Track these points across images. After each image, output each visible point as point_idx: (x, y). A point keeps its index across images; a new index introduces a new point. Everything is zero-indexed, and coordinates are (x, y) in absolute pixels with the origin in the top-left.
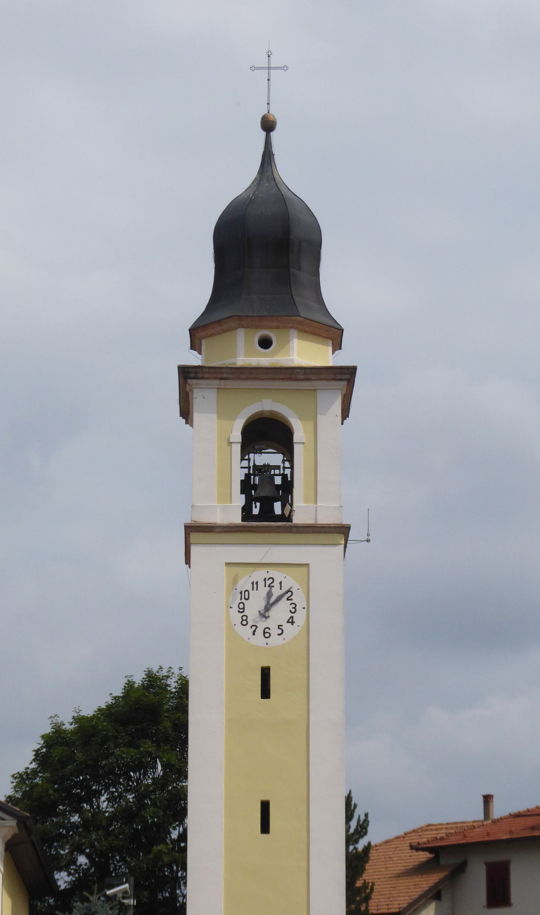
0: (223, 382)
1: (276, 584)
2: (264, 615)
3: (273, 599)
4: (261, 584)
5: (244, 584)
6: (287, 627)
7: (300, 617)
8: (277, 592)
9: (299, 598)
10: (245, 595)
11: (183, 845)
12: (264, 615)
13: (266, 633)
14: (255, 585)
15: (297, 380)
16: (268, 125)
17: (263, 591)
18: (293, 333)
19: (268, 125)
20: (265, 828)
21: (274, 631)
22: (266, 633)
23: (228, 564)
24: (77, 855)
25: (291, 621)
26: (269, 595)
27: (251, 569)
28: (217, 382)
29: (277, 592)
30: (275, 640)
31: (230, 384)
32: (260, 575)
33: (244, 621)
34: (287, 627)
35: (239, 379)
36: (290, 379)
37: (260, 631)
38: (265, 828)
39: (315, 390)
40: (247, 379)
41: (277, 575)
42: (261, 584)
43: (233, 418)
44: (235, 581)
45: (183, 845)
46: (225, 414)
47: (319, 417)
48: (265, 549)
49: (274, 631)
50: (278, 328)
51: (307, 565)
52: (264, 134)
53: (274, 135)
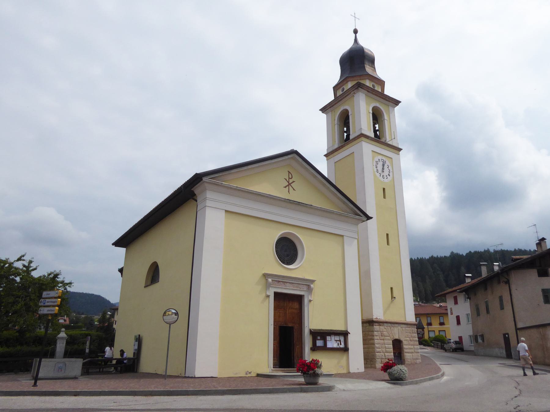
6: (388, 176)
16: (356, 32)
19: (356, 32)
28: (366, 92)
35: (372, 93)
37: (382, 176)
48: (381, 149)
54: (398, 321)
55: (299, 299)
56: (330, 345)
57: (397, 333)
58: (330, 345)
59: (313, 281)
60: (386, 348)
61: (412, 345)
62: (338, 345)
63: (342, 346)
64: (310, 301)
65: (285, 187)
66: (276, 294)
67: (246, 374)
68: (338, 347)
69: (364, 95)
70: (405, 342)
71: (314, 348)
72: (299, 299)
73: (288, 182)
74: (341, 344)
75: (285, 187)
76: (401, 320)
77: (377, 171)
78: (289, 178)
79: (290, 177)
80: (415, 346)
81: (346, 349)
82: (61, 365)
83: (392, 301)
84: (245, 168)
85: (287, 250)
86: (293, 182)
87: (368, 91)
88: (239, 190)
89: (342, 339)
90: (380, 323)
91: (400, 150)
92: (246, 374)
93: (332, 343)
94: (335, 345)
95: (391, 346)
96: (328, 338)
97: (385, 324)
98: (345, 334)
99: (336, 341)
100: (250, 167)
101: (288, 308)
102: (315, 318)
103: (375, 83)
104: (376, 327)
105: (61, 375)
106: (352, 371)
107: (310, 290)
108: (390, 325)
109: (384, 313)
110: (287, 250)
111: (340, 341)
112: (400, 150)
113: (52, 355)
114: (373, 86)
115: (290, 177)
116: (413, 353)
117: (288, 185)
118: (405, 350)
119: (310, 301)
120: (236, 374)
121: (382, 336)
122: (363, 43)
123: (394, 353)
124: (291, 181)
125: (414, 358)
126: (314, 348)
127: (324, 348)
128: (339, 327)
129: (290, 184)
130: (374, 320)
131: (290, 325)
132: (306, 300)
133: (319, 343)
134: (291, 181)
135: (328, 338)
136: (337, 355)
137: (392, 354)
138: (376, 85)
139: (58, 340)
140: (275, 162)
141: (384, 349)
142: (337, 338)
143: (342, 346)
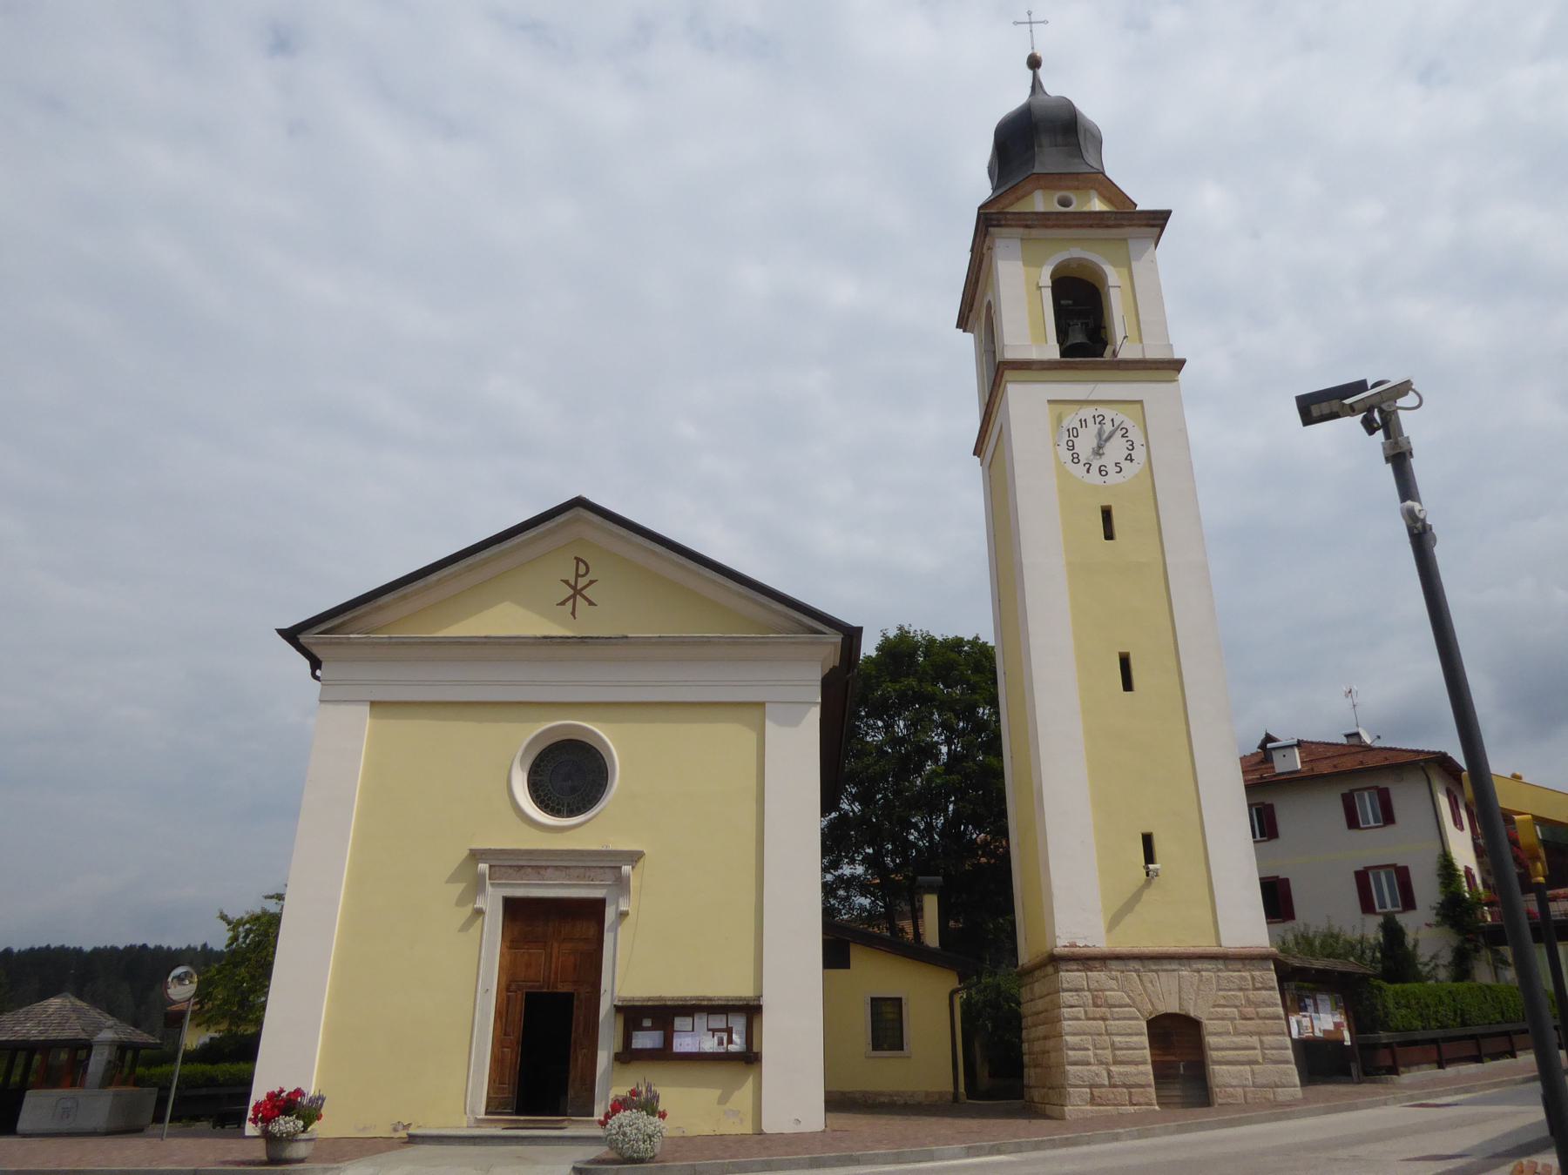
0: (1027, 231)
1: (1107, 421)
2: (1098, 451)
3: (1105, 436)
4: (1090, 421)
5: (1071, 421)
6: (1125, 465)
7: (1139, 454)
8: (1108, 428)
9: (1135, 435)
10: (1073, 433)
11: (829, 877)
12: (1098, 451)
13: (1102, 471)
14: (1084, 423)
15: (1108, 226)
16: (1034, 63)
17: (1093, 428)
18: (1093, 193)
19: (1034, 63)
20: (1128, 685)
21: (1112, 469)
22: (1102, 471)
23: (1049, 402)
24: (859, 755)
25: (1130, 458)
26: (1100, 434)
27: (1076, 407)
28: (1021, 230)
29: (1108, 428)
30: (1113, 478)
31: (1034, 232)
32: (1087, 412)
33: (1076, 459)
34: (1125, 465)
35: (1046, 227)
36: (1099, 226)
37: (1094, 469)
38: (1128, 685)
39: (762, 704)
40: (1053, 226)
41: (1109, 412)
42: (1090, 421)
43: (1040, 265)
44: (1059, 419)
45: (829, 877)
46: (1031, 262)
47: (1134, 264)
48: (1090, 386)
49: (1112, 469)
50: (1077, 188)
51: (1141, 402)
52: (1030, 73)
53: (1041, 72)
54: (1181, 950)
55: (593, 911)
57: (1169, 993)
58: (683, 1044)
59: (635, 857)
60: (1114, 1047)
61: (1251, 1034)
62: (721, 1043)
63: (738, 1044)
64: (624, 915)
65: (563, 603)
66: (513, 908)
67: (395, 1130)
68: (721, 1050)
69: (1016, 245)
70: (1209, 1025)
71: (627, 1056)
72: (593, 911)
73: (574, 588)
74: (730, 1041)
75: (563, 603)
76: (1205, 944)
77: (1076, 459)
78: (577, 575)
80: (1268, 1039)
81: (750, 1058)
82: (69, 1104)
83: (1148, 883)
84: (420, 583)
85: (568, 776)
86: (592, 582)
87: (1027, 226)
88: (397, 644)
89: (738, 1023)
90: (1087, 960)
91: (1178, 365)
92: (395, 1130)
93: (693, 1038)
94: (709, 1044)
95: (1145, 1040)
96: (680, 1023)
97: (1113, 964)
98: (751, 1011)
99: (714, 1031)
100: (433, 577)
101: (552, 940)
102: (633, 968)
103: (1068, 188)
104: (1070, 977)
105: (65, 1126)
106: (769, 1127)
107: (622, 884)
108: (1136, 965)
109: (1114, 922)
110: (568, 776)
112: (1178, 365)
114: (1065, 202)
115: (582, 569)
116: (1256, 1062)
117: (573, 597)
118: (1215, 1055)
119: (624, 915)
120: (364, 1129)
121: (1096, 1005)
122: (1054, 87)
123: (1154, 1063)
124: (582, 582)
125: (1259, 1081)
126: (627, 1056)
127: (664, 1054)
128: (736, 988)
129: (577, 592)
130: (1057, 951)
131: (563, 988)
132: (610, 914)
136: (721, 1073)
137: (1149, 1068)
138: (1071, 195)
141: (1107, 1054)
142: (719, 1022)
143: (738, 1044)
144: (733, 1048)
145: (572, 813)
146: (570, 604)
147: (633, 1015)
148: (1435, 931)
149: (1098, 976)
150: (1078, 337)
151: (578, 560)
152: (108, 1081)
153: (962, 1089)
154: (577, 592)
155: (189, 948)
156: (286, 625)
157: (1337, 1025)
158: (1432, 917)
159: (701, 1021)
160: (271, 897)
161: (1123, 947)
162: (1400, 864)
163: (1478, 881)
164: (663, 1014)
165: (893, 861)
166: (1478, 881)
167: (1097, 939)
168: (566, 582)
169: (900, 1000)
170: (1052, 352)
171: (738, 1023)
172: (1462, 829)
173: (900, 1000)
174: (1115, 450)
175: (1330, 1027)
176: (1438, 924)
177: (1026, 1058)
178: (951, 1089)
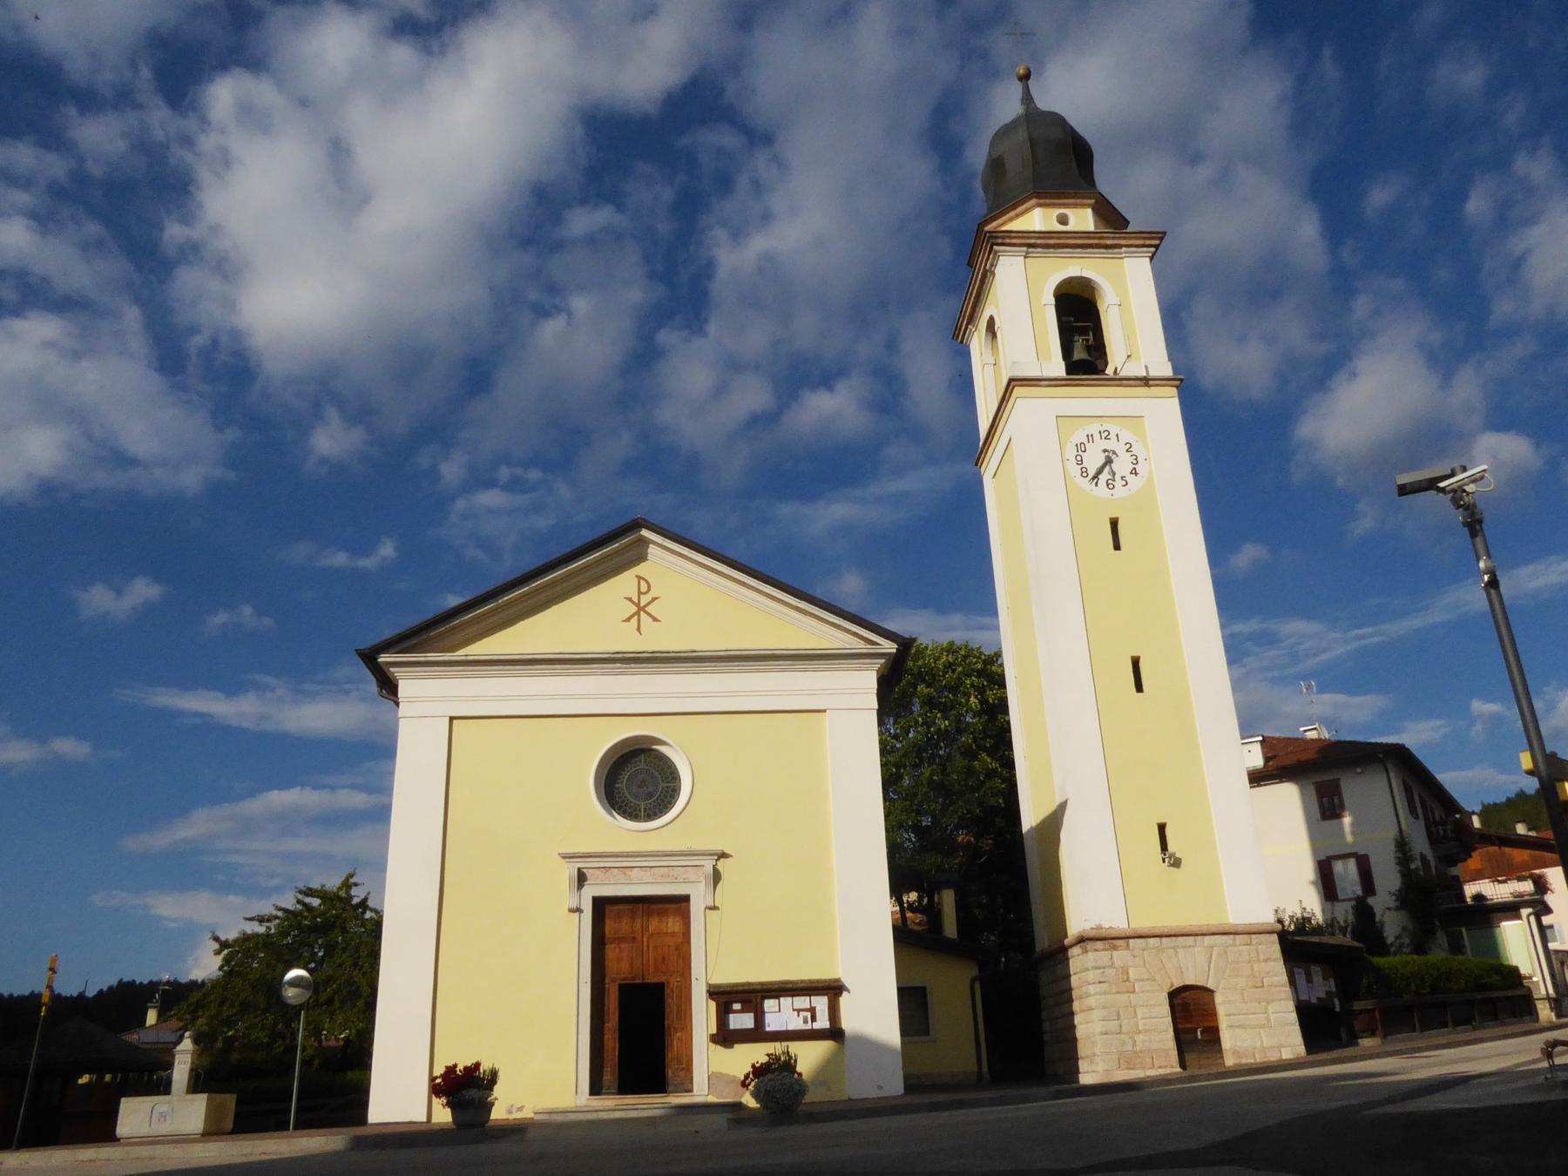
6: (1130, 478)
7: (1071, 452)
10: (1082, 448)
14: (1090, 437)
25: (1134, 472)
32: (1094, 428)
33: (1084, 473)
34: (1130, 478)
56: (773, 1023)
57: (1191, 967)
58: (773, 1023)
62: (805, 1021)
63: (823, 1023)
65: (628, 620)
68: (809, 1026)
73: (638, 605)
74: (814, 1019)
75: (628, 620)
78: (640, 593)
79: (644, 587)
86: (654, 599)
89: (821, 1003)
92: (510, 1112)
94: (797, 1023)
96: (769, 1004)
99: (799, 1011)
102: (719, 954)
110: (636, 778)
111: (812, 1010)
113: (164, 1088)
114: (1063, 220)
115: (644, 587)
117: (637, 613)
124: (644, 600)
129: (641, 609)
133: (741, 1020)
134: (644, 600)
135: (769, 1004)
139: (1075, 952)
140: (617, 553)
142: (802, 1002)
143: (823, 1023)
144: (817, 1026)
145: (651, 815)
146: (635, 619)
147: (724, 998)
148: (1394, 914)
149: (1120, 957)
150: (1079, 354)
151: (639, 578)
152: (197, 1084)
153: (985, 1069)
154: (641, 609)
155: (121, 983)
156: (362, 647)
157: (1328, 993)
158: (1392, 902)
159: (786, 1002)
160: (251, 919)
161: (1142, 923)
162: (1361, 852)
163: (1433, 864)
164: (752, 996)
165: (296, 982)
166: (1433, 864)
167: (1115, 920)
168: (630, 600)
169: (924, 989)
170: (1058, 368)
171: (821, 1003)
172: (1417, 817)
173: (924, 989)
174: (1094, 460)
175: (1323, 995)
176: (1397, 909)
177: (1047, 1037)
178: (975, 1069)
